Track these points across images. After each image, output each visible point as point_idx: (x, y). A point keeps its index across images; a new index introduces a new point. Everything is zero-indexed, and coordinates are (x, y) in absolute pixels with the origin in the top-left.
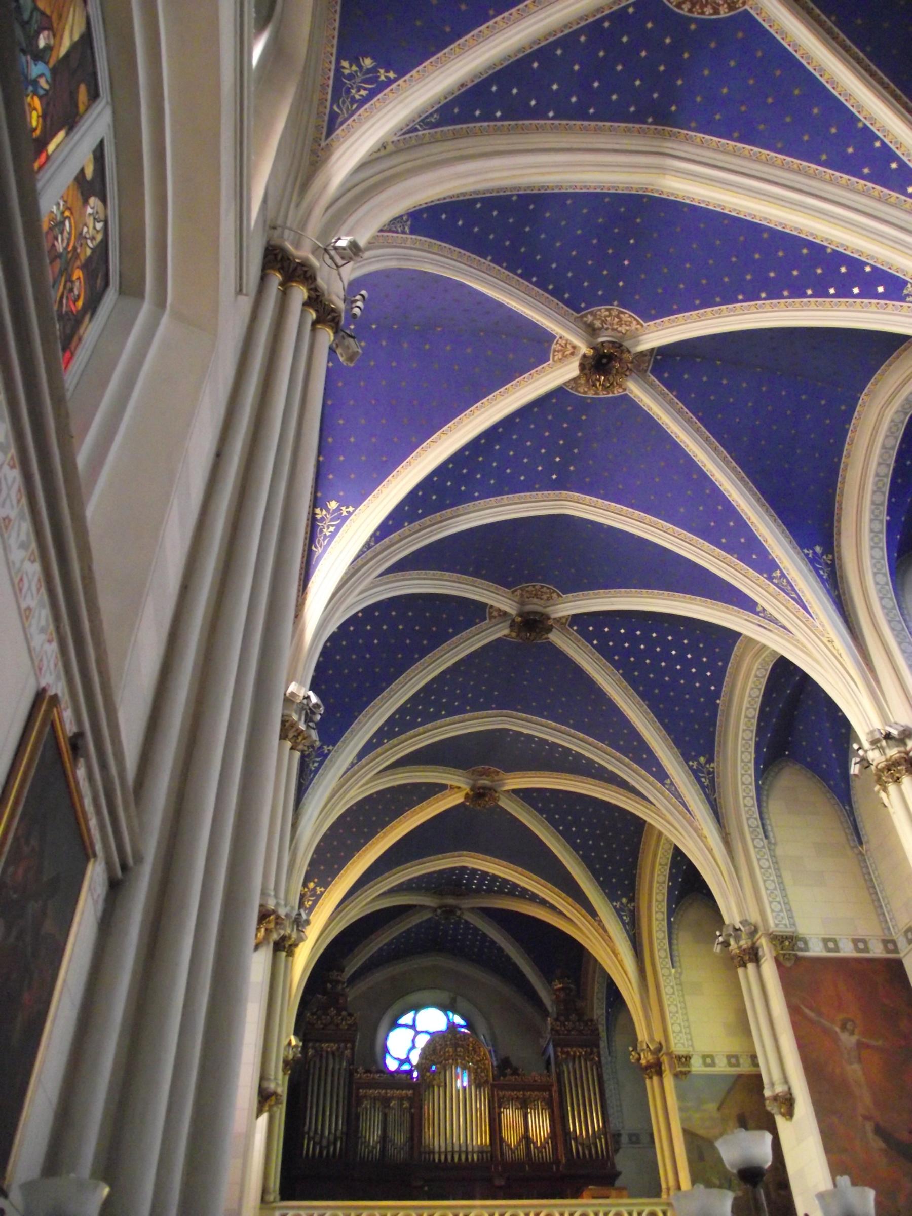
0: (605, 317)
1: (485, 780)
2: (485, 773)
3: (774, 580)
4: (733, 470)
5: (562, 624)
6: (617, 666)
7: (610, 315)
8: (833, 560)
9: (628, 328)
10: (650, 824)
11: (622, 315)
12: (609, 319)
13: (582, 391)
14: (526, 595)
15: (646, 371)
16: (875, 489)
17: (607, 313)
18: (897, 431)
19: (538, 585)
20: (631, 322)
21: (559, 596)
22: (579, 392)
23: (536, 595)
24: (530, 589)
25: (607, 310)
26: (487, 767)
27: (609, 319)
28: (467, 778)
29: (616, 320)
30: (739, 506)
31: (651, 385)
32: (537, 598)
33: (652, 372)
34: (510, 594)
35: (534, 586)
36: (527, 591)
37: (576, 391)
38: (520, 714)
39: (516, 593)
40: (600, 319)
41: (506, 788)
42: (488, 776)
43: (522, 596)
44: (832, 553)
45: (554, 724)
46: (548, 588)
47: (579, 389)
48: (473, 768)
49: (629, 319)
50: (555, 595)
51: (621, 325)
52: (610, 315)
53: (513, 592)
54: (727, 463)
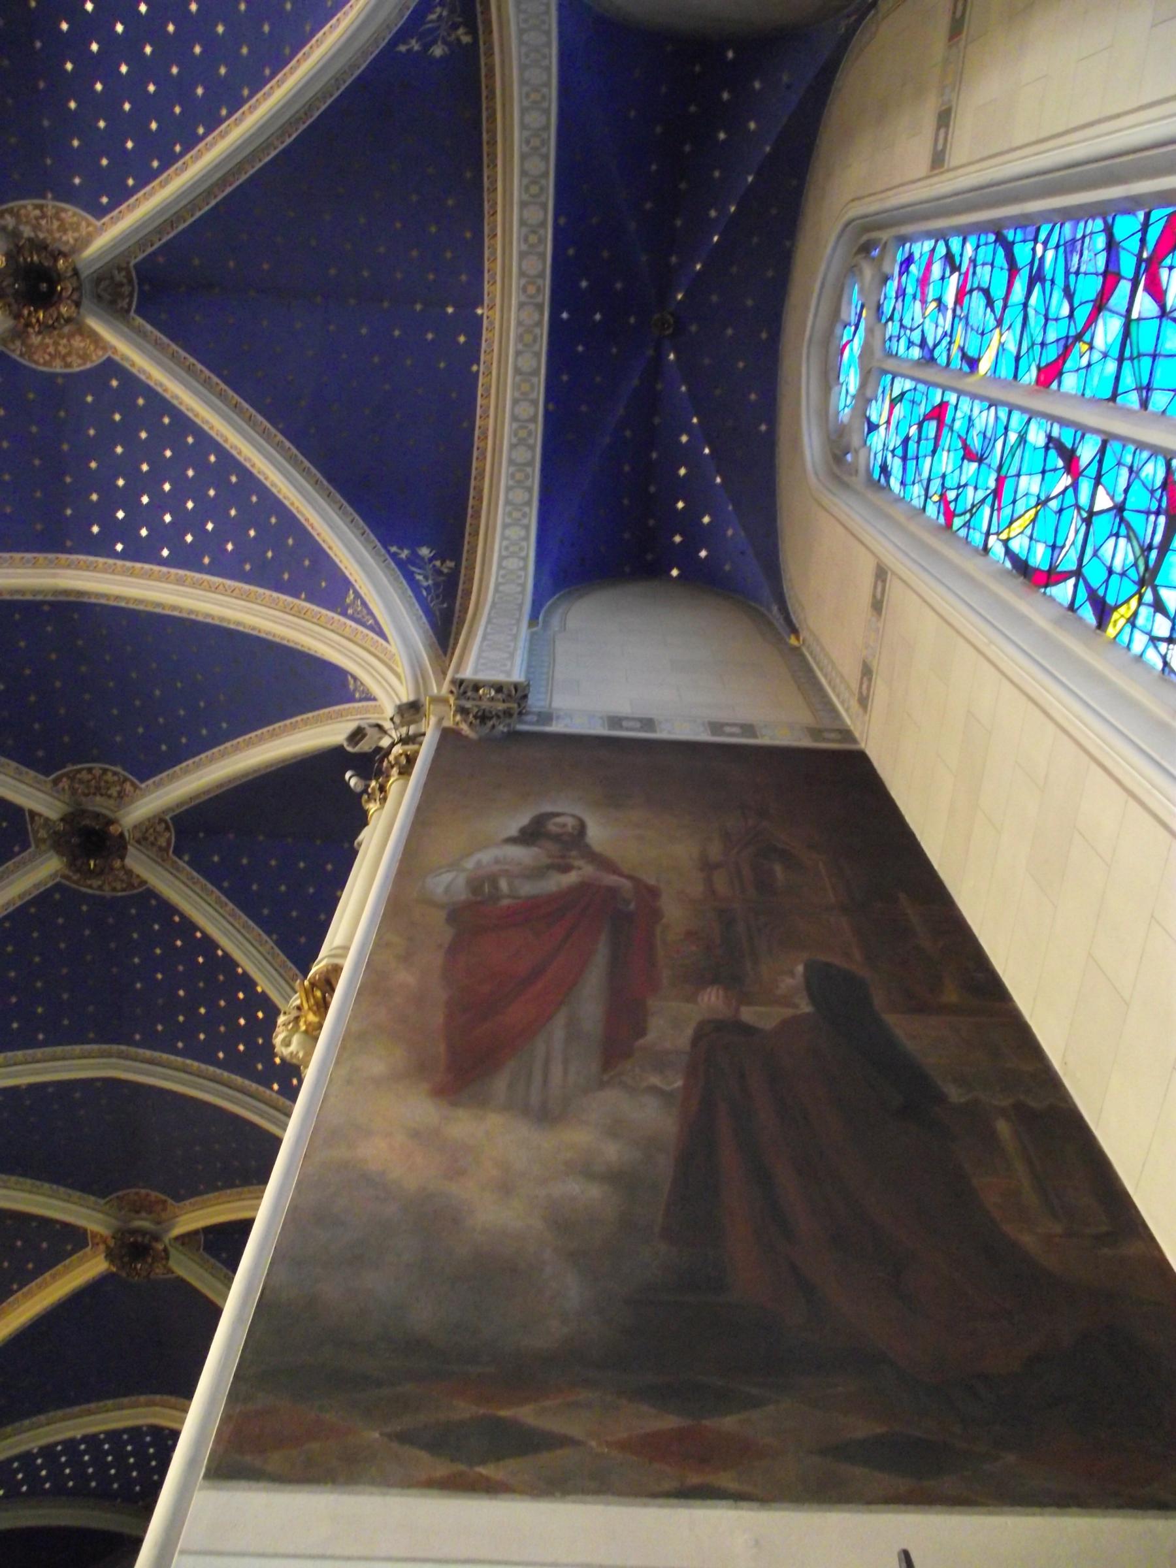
0: (37, 218)
1: (145, 1219)
2: (138, 1208)
3: (371, 622)
4: (278, 446)
5: (161, 849)
6: (266, 925)
7: (43, 216)
8: (455, 573)
9: (76, 235)
10: (263, 1191)
11: (63, 215)
12: (43, 222)
13: (41, 361)
14: (81, 788)
15: (128, 311)
16: (514, 440)
17: (37, 212)
18: (535, 340)
19: (97, 767)
20: (78, 224)
21: (135, 787)
22: (37, 363)
23: (98, 788)
24: (84, 775)
25: (36, 207)
26: (143, 1191)
27: (43, 222)
28: (107, 1214)
29: (56, 224)
30: (197, 415)
31: (139, 331)
32: (102, 795)
33: (138, 312)
34: (49, 786)
35: (90, 770)
36: (81, 782)
37: (31, 359)
38: (141, 1051)
39: (61, 785)
40: (27, 223)
41: (177, 1231)
42: (150, 1212)
43: (74, 792)
44: (457, 558)
45: (196, 1064)
46: (115, 773)
47: (36, 357)
48: (120, 1193)
49: (75, 219)
50: (128, 786)
51: (65, 231)
52: (43, 216)
53: (56, 782)
54: (268, 438)
